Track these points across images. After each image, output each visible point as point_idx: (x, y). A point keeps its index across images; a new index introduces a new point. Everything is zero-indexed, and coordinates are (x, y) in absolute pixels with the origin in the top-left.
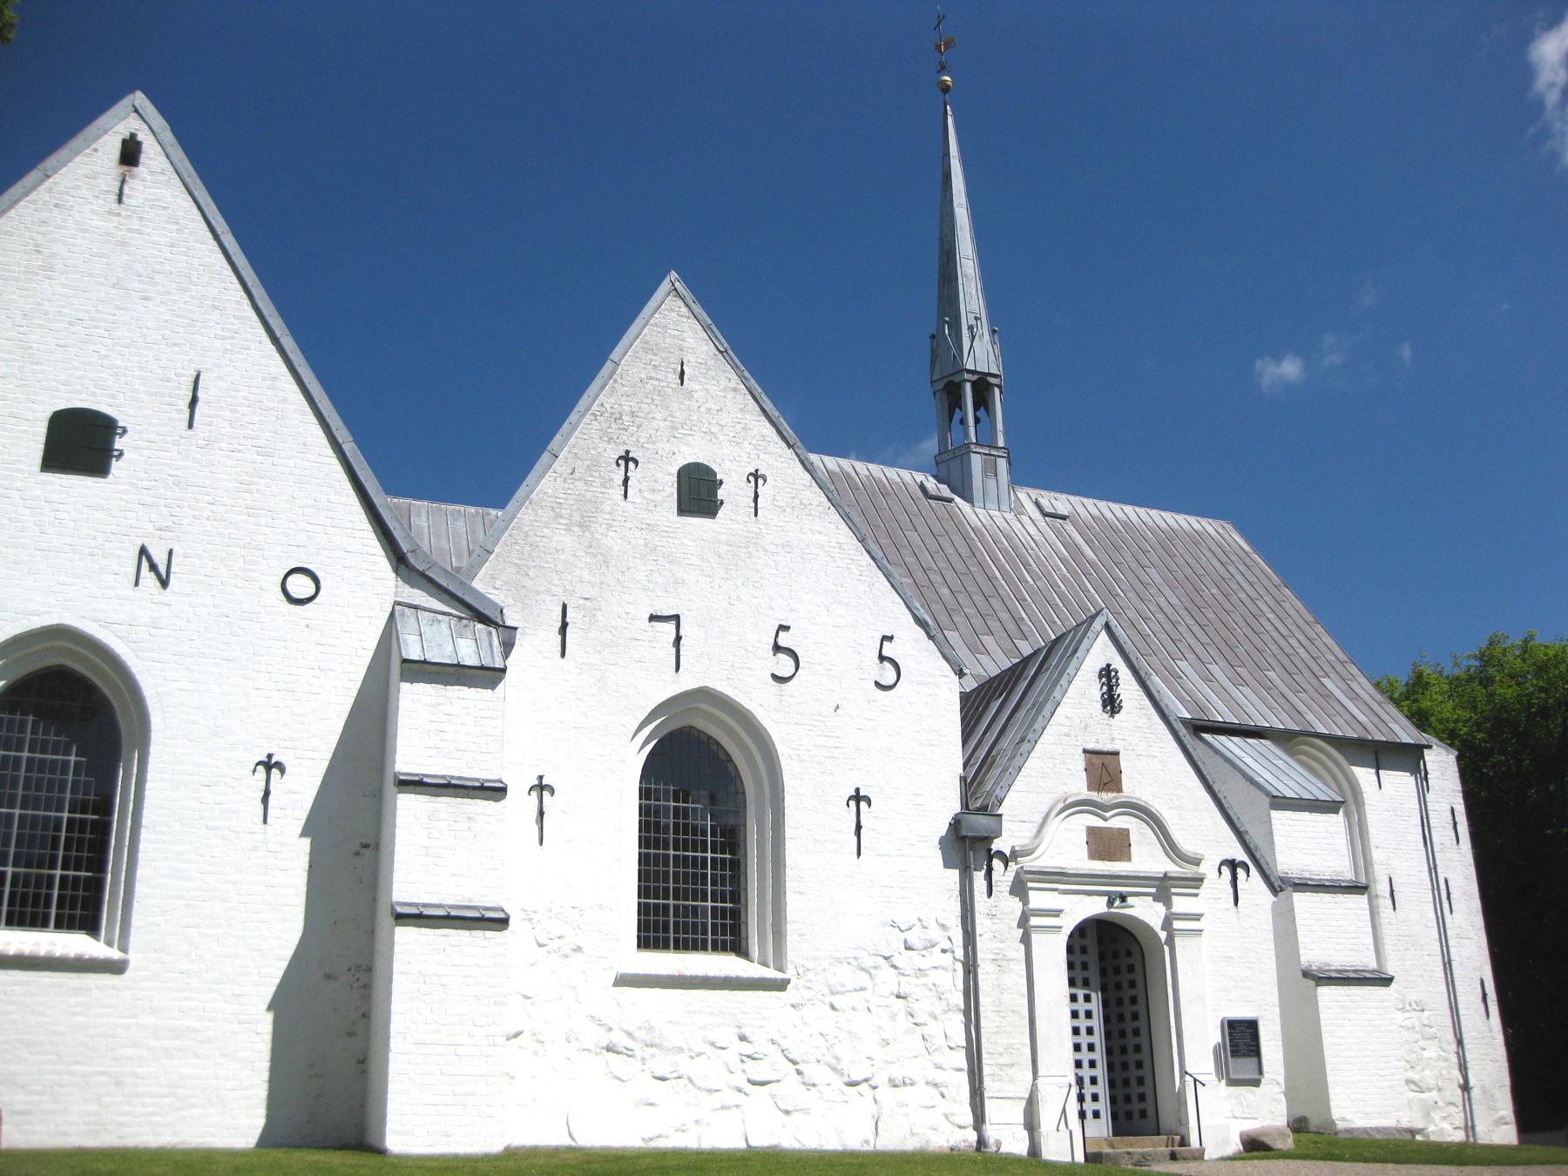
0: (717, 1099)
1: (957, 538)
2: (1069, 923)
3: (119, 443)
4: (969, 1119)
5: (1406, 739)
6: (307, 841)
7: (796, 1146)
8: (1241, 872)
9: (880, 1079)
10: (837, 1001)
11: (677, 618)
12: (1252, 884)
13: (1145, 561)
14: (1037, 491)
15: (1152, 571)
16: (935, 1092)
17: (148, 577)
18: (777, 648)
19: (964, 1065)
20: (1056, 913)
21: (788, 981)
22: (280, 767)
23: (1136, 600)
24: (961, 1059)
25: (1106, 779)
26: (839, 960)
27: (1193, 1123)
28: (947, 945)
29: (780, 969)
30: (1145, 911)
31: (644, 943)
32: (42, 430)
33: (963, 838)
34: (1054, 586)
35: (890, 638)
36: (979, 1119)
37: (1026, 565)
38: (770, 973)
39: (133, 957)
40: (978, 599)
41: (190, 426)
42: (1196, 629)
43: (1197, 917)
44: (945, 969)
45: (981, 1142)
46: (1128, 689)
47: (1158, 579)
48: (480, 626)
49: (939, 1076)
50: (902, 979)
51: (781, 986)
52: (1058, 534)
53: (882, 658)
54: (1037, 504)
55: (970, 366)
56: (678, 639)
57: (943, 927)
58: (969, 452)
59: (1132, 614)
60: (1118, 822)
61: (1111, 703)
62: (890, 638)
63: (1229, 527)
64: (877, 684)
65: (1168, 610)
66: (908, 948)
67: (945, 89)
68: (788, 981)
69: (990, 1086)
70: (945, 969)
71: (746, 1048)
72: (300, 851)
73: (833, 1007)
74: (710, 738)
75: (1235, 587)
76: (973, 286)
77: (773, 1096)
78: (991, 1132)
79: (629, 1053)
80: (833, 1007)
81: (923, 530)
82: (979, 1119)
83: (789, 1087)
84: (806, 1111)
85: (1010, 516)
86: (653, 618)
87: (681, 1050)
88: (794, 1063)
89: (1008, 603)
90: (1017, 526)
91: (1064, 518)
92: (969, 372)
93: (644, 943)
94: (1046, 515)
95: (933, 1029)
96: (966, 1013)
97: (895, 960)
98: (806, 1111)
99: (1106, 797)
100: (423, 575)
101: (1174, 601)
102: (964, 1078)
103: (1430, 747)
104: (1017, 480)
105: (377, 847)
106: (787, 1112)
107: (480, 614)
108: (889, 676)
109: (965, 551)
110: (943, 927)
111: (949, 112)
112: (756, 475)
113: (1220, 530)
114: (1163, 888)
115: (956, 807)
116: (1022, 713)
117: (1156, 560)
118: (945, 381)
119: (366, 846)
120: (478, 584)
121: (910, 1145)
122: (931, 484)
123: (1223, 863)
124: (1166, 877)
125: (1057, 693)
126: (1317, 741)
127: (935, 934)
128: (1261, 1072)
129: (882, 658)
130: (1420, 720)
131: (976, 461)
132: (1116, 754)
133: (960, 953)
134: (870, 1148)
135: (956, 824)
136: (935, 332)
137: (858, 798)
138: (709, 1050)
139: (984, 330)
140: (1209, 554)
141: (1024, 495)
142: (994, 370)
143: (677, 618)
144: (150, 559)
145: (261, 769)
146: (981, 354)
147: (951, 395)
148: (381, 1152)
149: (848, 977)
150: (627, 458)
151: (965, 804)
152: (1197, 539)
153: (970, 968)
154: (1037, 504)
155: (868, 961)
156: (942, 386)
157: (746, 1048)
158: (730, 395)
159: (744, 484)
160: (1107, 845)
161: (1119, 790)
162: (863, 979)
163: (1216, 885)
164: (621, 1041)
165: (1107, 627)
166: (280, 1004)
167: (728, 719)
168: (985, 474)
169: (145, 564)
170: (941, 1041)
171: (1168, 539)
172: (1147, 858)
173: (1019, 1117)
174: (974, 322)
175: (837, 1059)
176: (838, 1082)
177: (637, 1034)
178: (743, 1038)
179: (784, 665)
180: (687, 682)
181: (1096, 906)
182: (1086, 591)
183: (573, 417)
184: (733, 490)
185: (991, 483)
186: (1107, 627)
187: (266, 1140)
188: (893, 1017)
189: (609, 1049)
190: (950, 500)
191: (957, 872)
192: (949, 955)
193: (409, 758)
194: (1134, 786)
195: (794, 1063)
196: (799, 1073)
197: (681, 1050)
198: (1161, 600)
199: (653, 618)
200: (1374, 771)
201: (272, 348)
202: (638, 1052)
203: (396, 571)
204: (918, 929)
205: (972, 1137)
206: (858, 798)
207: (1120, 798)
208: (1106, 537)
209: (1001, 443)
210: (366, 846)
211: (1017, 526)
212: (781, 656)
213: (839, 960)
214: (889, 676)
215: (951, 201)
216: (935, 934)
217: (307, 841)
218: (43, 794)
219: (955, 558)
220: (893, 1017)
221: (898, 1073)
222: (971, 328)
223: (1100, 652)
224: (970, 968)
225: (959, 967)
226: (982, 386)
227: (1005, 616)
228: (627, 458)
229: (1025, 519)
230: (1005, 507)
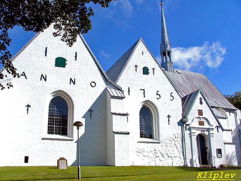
0: (152, 159)
2: (197, 134)
3: (66, 62)
5: (234, 109)
8: (219, 128)
11: (144, 90)
12: (220, 129)
17: (43, 79)
18: (157, 94)
20: (195, 133)
25: (201, 113)
27: (214, 163)
30: (206, 133)
32: (54, 61)
35: (172, 93)
43: (213, 134)
46: (203, 101)
49: (180, 156)
51: (159, 143)
53: (171, 96)
54: (177, 71)
60: (202, 120)
61: (201, 103)
62: (172, 93)
64: (171, 100)
71: (155, 152)
73: (166, 146)
79: (140, 152)
80: (166, 146)
86: (141, 90)
88: (161, 154)
92: (167, 50)
93: (141, 137)
99: (201, 117)
103: (237, 110)
106: (161, 161)
107: (119, 89)
114: (208, 130)
123: (216, 126)
124: (209, 128)
126: (221, 108)
128: (222, 156)
130: (235, 105)
132: (202, 110)
143: (144, 90)
144: (43, 76)
145: (90, 111)
149: (168, 142)
154: (177, 71)
157: (155, 152)
160: (201, 123)
161: (203, 115)
163: (215, 130)
164: (139, 151)
167: (151, 105)
169: (42, 77)
172: (206, 126)
178: (155, 150)
179: (158, 97)
181: (199, 132)
184: (151, 71)
194: (204, 115)
195: (161, 154)
199: (141, 90)
200: (229, 113)
201: (86, 48)
202: (141, 152)
207: (203, 116)
212: (158, 95)
220: (174, 147)
223: (199, 96)
229: (175, 73)
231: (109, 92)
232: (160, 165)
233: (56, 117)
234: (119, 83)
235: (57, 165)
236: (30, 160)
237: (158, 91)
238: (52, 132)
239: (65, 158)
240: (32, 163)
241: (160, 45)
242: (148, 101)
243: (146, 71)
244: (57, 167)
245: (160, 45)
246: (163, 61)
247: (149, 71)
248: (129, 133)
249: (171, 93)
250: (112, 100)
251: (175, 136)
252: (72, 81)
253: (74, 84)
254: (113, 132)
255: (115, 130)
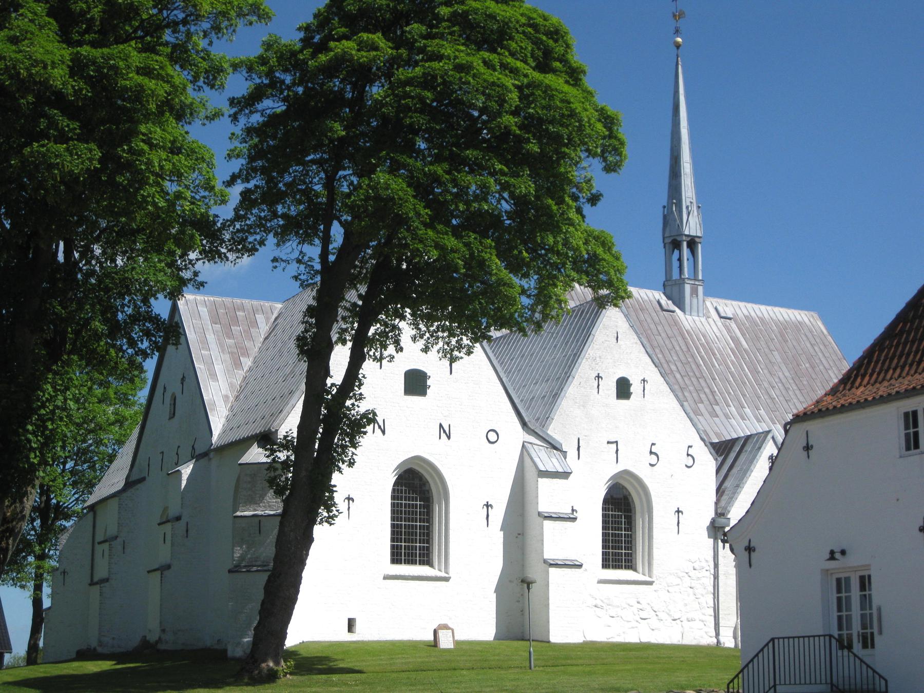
1: (680, 339)
3: (429, 382)
4: (714, 634)
6: (502, 533)
7: (656, 642)
9: (684, 619)
10: (670, 589)
11: (617, 442)
13: (772, 347)
14: (716, 300)
15: (776, 353)
16: (702, 623)
18: (651, 453)
19: (713, 614)
21: (654, 582)
22: (491, 506)
23: (768, 375)
24: (711, 612)
26: (671, 574)
28: (708, 568)
29: (650, 577)
31: (605, 565)
33: (715, 527)
34: (728, 368)
36: (717, 634)
37: (714, 354)
38: (647, 579)
39: (450, 575)
40: (694, 379)
41: (451, 373)
42: (797, 392)
44: (707, 577)
45: (718, 642)
47: (779, 360)
48: (555, 451)
49: (704, 618)
50: (692, 581)
51: (651, 583)
52: (725, 326)
53: (688, 455)
54: (716, 309)
55: (687, 233)
56: (617, 450)
57: (707, 561)
58: (684, 283)
59: (766, 385)
63: (816, 316)
65: (784, 380)
66: (694, 569)
67: (678, 46)
68: (654, 582)
69: (722, 622)
70: (707, 577)
71: (639, 606)
72: (501, 535)
74: (623, 486)
75: (818, 361)
76: (689, 180)
77: (648, 624)
78: (722, 639)
79: (602, 608)
81: (663, 335)
82: (717, 634)
83: (654, 622)
84: (659, 630)
85: (703, 320)
86: (608, 442)
87: (618, 607)
89: (708, 381)
90: (708, 327)
91: (730, 319)
92: (686, 236)
93: (605, 565)
94: (721, 317)
95: (702, 600)
96: (714, 594)
97: (690, 574)
98: (659, 630)
100: (533, 431)
101: (787, 374)
102: (712, 619)
104: (707, 294)
105: (523, 534)
107: (554, 446)
108: (690, 462)
109: (684, 348)
110: (707, 561)
111: (680, 63)
112: (644, 380)
113: (812, 320)
115: (713, 515)
116: (734, 470)
117: (778, 345)
118: (672, 238)
119: (519, 534)
120: (549, 432)
121: (694, 643)
122: (664, 300)
125: (752, 467)
127: (704, 564)
129: (688, 455)
131: (688, 288)
133: (712, 571)
134: (680, 643)
135: (713, 522)
136: (666, 204)
137: (678, 511)
138: (627, 606)
139: (694, 209)
140: (805, 338)
141: (711, 303)
142: (699, 234)
143: (617, 442)
145: (485, 507)
146: (692, 226)
147: (676, 245)
148: (549, 642)
150: (598, 377)
151: (716, 513)
152: (798, 327)
153: (716, 577)
155: (681, 574)
156: (670, 241)
157: (639, 606)
158: (635, 346)
159: (639, 384)
162: (678, 581)
164: (599, 603)
165: (773, 438)
166: (498, 590)
168: (691, 295)
170: (705, 605)
171: (784, 327)
173: (732, 634)
174: (689, 204)
175: (670, 610)
176: (670, 620)
177: (605, 601)
178: (638, 603)
179: (653, 459)
180: (620, 467)
182: (743, 370)
183: (579, 360)
184: (635, 388)
185: (695, 301)
186: (773, 438)
187: (497, 637)
188: (689, 595)
189: (595, 606)
190: (673, 312)
191: (712, 540)
192: (708, 572)
193: (545, 505)
196: (657, 615)
197: (618, 607)
198: (780, 374)
199: (608, 442)
202: (605, 608)
203: (523, 428)
204: (698, 562)
205: (715, 641)
206: (678, 511)
208: (752, 328)
209: (700, 278)
210: (519, 534)
211: (708, 327)
213: (671, 574)
214: (690, 462)
215: (679, 115)
216: (704, 564)
217: (333, 483)
218: (411, 516)
219: (680, 353)
220: (689, 595)
221: (690, 616)
222: (687, 207)
224: (716, 577)
225: (712, 577)
226: (692, 243)
227: (707, 390)
228: (598, 377)
229: (710, 320)
230: (701, 314)
231: (532, 459)
232: (844, 372)
233: (416, 525)
234: (554, 431)
235: (432, 638)
236: (358, 626)
237: (653, 444)
238: (397, 560)
239: (451, 625)
240: (363, 634)
241: (664, 207)
242: (626, 473)
243: (623, 389)
244: (433, 644)
245: (664, 207)
246: (671, 276)
247: (632, 389)
248: (580, 566)
249: (690, 447)
250: (543, 483)
251: (694, 564)
252: (445, 431)
253: (449, 437)
254: (545, 561)
255: (549, 554)
